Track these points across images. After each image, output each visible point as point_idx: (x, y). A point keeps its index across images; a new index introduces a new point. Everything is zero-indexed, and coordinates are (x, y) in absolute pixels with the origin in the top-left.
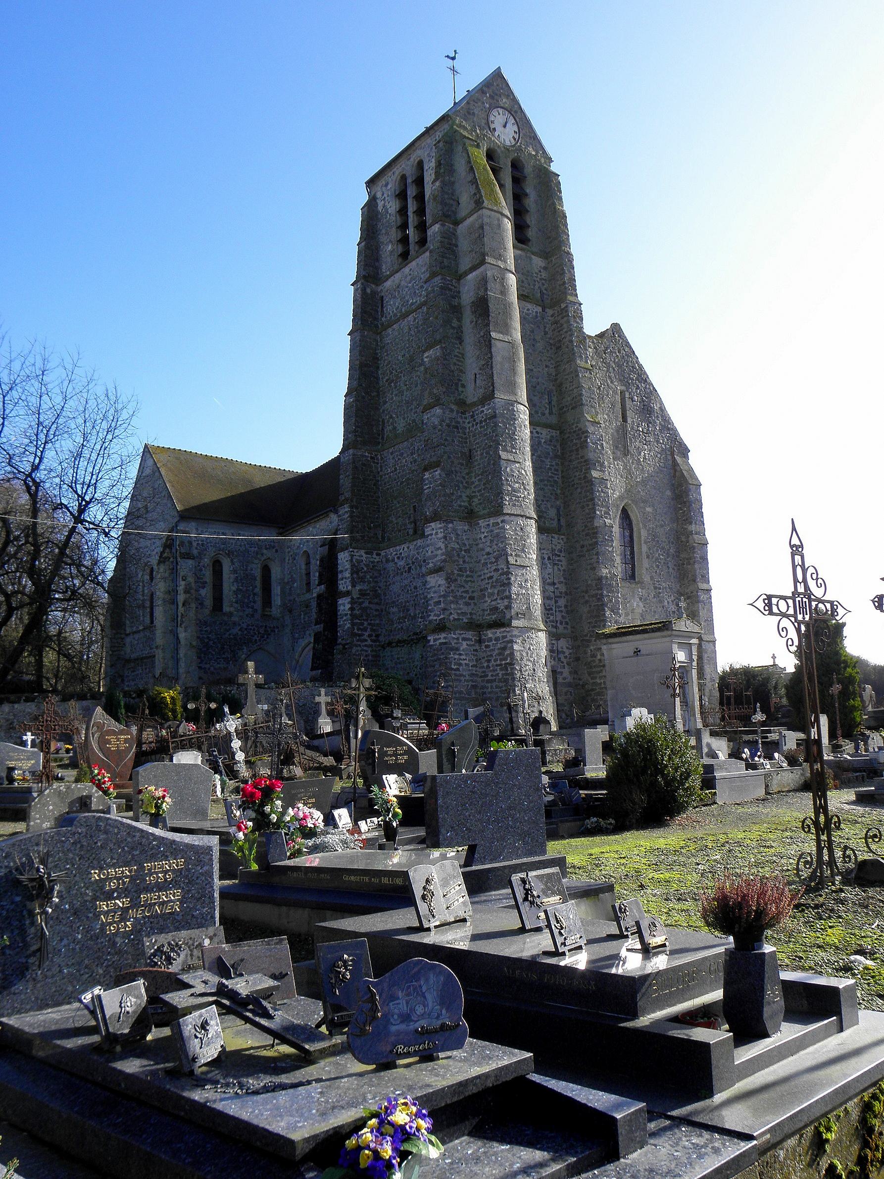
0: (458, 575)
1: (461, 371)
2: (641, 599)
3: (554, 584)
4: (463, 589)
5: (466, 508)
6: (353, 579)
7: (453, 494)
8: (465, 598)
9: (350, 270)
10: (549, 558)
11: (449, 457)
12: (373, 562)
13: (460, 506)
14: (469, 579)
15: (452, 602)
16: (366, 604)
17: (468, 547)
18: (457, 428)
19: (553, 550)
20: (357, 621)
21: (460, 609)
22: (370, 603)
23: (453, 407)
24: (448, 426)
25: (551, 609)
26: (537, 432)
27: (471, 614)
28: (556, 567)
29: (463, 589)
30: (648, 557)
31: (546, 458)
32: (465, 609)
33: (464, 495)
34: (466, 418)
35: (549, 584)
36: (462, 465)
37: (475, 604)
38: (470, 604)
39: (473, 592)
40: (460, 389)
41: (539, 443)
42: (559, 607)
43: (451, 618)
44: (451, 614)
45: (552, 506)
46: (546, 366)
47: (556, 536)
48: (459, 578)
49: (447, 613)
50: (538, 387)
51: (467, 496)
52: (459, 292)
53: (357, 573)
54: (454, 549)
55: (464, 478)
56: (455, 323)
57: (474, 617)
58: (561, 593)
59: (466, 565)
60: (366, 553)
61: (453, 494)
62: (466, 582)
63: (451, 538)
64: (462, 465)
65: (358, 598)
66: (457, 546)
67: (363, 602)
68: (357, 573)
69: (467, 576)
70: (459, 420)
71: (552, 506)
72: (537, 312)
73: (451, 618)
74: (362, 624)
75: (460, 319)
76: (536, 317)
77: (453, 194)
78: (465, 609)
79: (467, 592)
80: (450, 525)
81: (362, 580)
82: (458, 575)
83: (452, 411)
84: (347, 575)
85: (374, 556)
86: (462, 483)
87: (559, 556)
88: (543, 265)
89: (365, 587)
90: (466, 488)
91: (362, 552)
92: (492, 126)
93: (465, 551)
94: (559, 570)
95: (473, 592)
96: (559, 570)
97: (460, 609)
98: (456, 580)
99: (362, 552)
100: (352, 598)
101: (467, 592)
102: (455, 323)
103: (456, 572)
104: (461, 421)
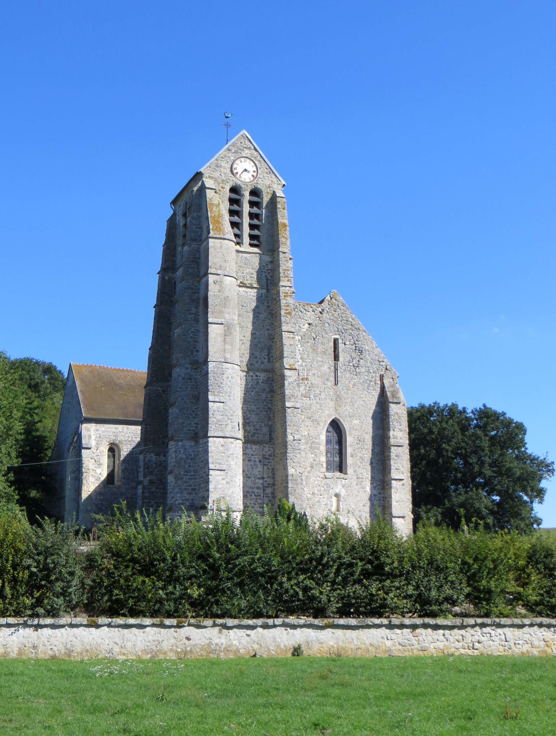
0: (184, 475)
1: (197, 342)
2: (343, 486)
3: (263, 478)
4: (187, 484)
5: (194, 430)
6: (144, 473)
7: (183, 423)
8: (188, 490)
9: (157, 263)
10: (260, 461)
11: (182, 399)
12: (161, 461)
13: (189, 430)
14: (193, 477)
15: (178, 493)
16: (154, 489)
17: (193, 456)
18: (190, 379)
19: (263, 455)
20: (147, 500)
21: (184, 497)
22: (156, 488)
23: (187, 365)
24: (183, 378)
25: (260, 495)
26: (257, 376)
27: (192, 500)
28: (265, 467)
29: (187, 484)
30: (352, 456)
31: (262, 392)
32: (188, 497)
33: (192, 423)
34: (198, 372)
35: (259, 478)
36: (192, 403)
37: (196, 494)
38: (192, 494)
39: (195, 486)
40: (195, 353)
41: (258, 383)
42: (267, 494)
43: (177, 502)
44: (177, 500)
45: (265, 425)
46: (267, 330)
47: (267, 446)
48: (185, 477)
49: (174, 499)
50: (259, 345)
51: (196, 423)
52: (199, 289)
53: (148, 468)
54: (181, 458)
55: (193, 411)
56: (193, 310)
57: (194, 502)
58: (269, 484)
59: (192, 469)
60: (155, 455)
61: (183, 423)
62: (190, 479)
63: (180, 452)
64: (192, 403)
65: (147, 485)
66: (184, 456)
67: (151, 488)
68: (148, 468)
69: (191, 476)
70: (193, 374)
71: (265, 425)
72: (262, 293)
73: (177, 502)
74: (150, 503)
75: (197, 308)
76: (262, 297)
77: (199, 225)
78: (188, 497)
79: (190, 486)
80: (180, 443)
81: (151, 473)
82: (184, 475)
83: (187, 368)
84: (142, 470)
85: (162, 456)
86: (192, 415)
87: (269, 459)
88: (270, 260)
89: (153, 477)
90: (195, 418)
91: (152, 455)
92: (235, 171)
93: (191, 459)
94: (268, 468)
95: (195, 486)
96: (268, 468)
97: (184, 497)
98: (182, 478)
99: (152, 455)
100: (144, 486)
101: (190, 486)
102: (193, 310)
103: (182, 473)
104: (194, 374)
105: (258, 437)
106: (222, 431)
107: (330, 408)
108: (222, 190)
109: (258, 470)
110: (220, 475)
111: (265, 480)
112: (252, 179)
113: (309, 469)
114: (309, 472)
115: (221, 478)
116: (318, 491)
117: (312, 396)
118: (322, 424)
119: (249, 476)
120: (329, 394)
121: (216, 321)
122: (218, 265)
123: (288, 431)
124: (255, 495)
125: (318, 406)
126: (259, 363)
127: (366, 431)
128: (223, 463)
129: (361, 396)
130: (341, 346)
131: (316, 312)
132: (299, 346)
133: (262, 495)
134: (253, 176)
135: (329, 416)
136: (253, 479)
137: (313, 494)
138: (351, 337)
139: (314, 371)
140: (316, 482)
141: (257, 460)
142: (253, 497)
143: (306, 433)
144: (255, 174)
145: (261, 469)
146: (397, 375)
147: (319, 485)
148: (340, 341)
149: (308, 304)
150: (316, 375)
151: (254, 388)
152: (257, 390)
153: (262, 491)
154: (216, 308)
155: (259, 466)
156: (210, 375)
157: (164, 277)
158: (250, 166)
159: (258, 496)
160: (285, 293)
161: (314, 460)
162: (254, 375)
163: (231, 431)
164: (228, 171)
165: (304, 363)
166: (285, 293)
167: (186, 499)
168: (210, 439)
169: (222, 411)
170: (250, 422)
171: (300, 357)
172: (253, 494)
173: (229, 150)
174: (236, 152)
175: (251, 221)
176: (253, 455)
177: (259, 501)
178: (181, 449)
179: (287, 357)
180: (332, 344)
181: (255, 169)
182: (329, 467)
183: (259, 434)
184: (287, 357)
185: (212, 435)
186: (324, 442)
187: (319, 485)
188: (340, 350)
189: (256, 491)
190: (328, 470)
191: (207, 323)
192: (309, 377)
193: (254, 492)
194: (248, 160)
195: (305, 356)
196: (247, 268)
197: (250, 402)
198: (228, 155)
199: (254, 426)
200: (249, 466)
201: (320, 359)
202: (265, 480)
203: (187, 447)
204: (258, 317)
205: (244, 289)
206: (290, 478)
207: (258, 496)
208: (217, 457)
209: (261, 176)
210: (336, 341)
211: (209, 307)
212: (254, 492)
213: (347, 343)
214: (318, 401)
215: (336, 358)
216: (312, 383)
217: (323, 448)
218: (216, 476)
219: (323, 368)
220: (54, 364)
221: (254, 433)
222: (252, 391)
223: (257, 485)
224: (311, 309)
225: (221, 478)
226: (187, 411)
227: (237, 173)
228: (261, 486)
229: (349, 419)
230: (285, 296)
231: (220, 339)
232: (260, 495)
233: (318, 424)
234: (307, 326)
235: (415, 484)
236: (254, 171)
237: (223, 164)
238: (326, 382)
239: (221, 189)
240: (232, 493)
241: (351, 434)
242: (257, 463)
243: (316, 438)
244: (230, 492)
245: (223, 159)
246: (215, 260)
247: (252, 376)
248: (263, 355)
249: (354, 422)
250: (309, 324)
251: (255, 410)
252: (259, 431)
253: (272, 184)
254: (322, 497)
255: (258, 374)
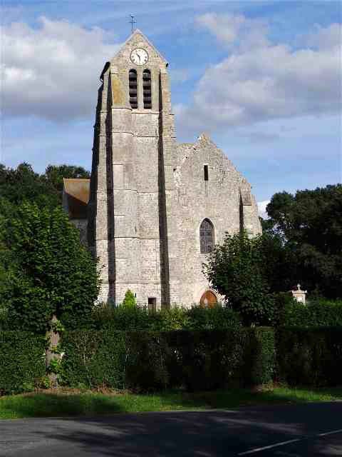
106: (124, 233)
139: (191, 189)
156: (115, 199)
158: (143, 54)
173: (128, 44)
175: (132, 90)
180: (203, 169)
186: (199, 235)
188: (209, 172)
190: (202, 252)
194: (142, 50)
205: (140, 138)
206: (170, 260)
215: (206, 178)
219: (197, 186)
220: (278, 192)
225: (123, 263)
235: (206, 301)
246: (117, 123)
253: (159, 66)
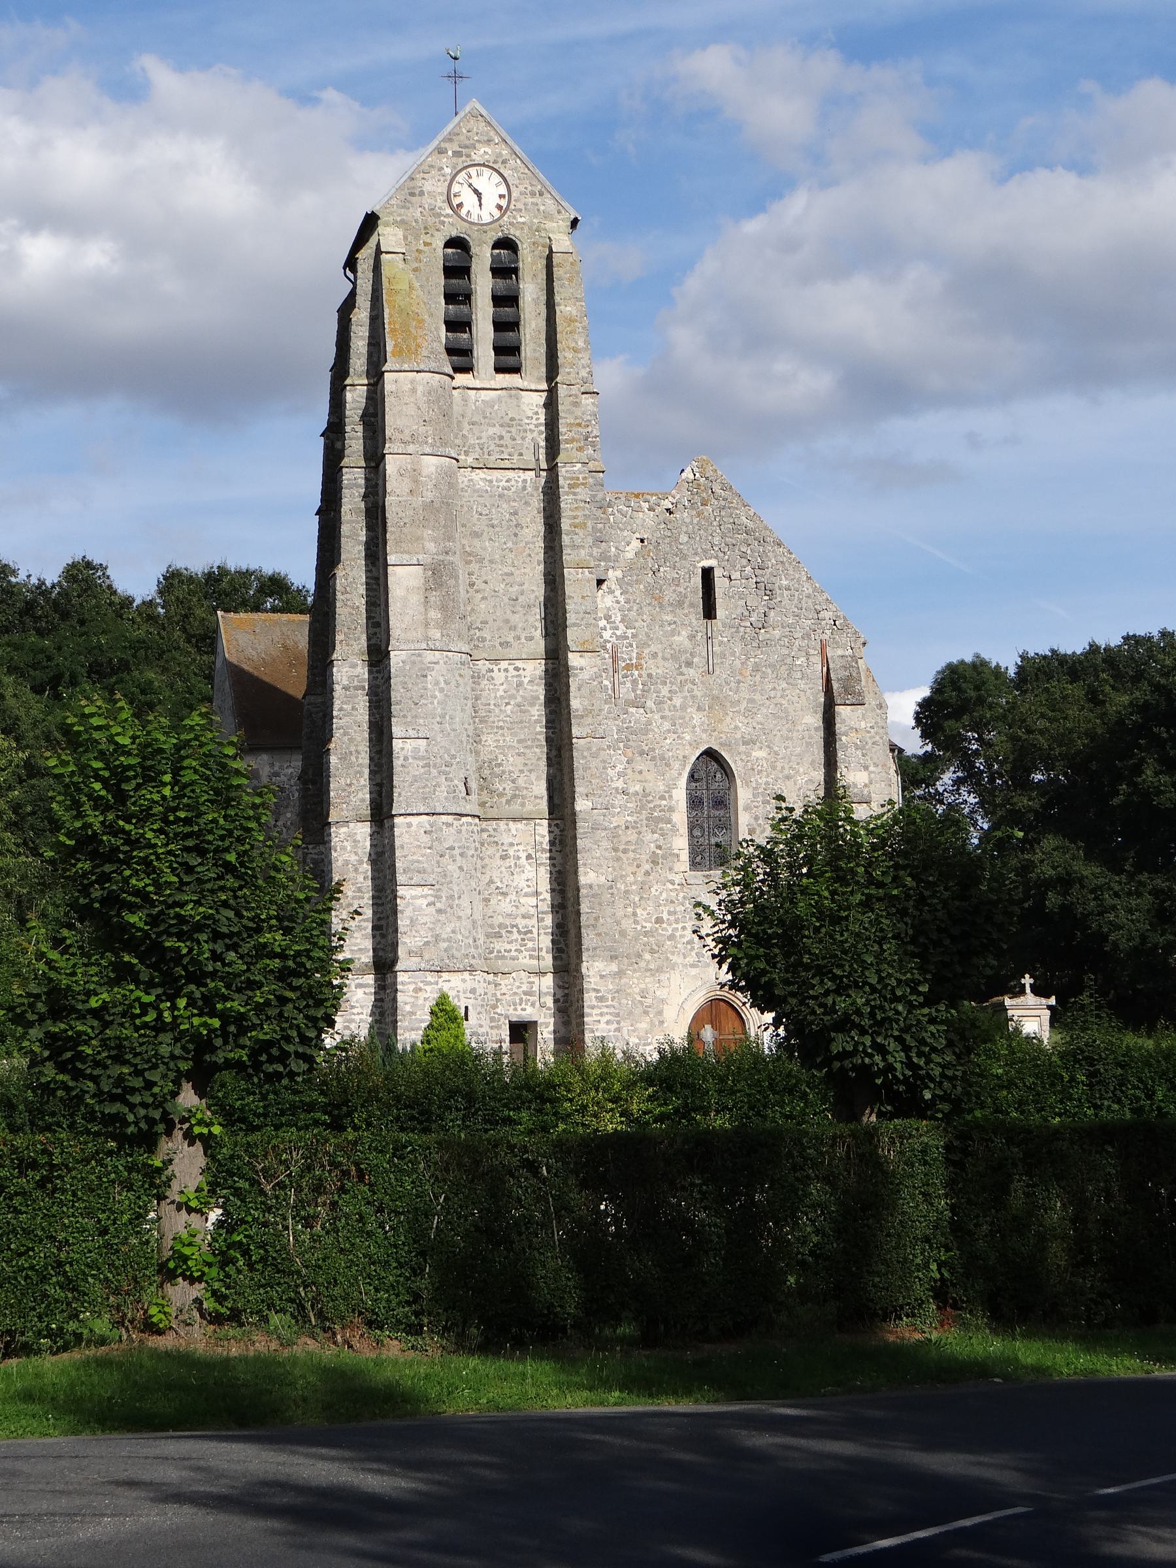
10: (529, 857)
25: (531, 932)
35: (526, 895)
105: (523, 805)
107: (694, 727)
108: (426, 249)
109: (524, 876)
110: (422, 896)
111: (541, 897)
112: (497, 214)
113: (647, 867)
114: (647, 873)
115: (425, 902)
116: (670, 913)
117: (650, 704)
118: (676, 765)
119: (504, 890)
120: (693, 697)
121: (406, 558)
122: (407, 432)
123: (577, 789)
124: (519, 932)
125: (667, 725)
126: (523, 640)
127: (786, 772)
128: (429, 870)
129: (772, 694)
130: (720, 584)
131: (658, 510)
132: (618, 593)
133: (535, 931)
134: (499, 207)
135: (694, 744)
136: (513, 897)
137: (659, 920)
138: (744, 562)
140: (664, 895)
141: (523, 855)
142: (516, 936)
143: (638, 788)
144: (504, 203)
145: (532, 875)
146: (862, 640)
147: (672, 902)
148: (718, 573)
149: (637, 496)
150: (660, 655)
151: (513, 697)
152: (519, 699)
153: (534, 921)
154: (405, 530)
155: (528, 867)
157: (333, 445)
158: (490, 186)
159: (526, 933)
160: (572, 479)
161: (659, 847)
162: (511, 668)
163: (446, 798)
164: (440, 202)
165: (629, 632)
166: (572, 479)
167: (360, 950)
168: (397, 820)
169: (423, 758)
170: (504, 772)
171: (619, 619)
172: (515, 930)
174: (457, 154)
176: (512, 845)
177: (530, 945)
178: (345, 843)
179: (575, 625)
180: (698, 580)
181: (503, 190)
182: (698, 859)
183: (524, 797)
184: (575, 625)
185: (403, 812)
187: (672, 902)
189: (521, 923)
190: (694, 865)
191: (386, 565)
192: (643, 662)
193: (516, 926)
195: (633, 614)
196: (489, 425)
197: (502, 728)
198: (439, 164)
199: (513, 782)
200: (503, 869)
201: (669, 618)
202: (541, 897)
203: (358, 837)
204: (516, 535)
206: (583, 892)
207: (526, 933)
208: (415, 858)
209: (520, 206)
210: (707, 574)
211: (390, 529)
212: (516, 926)
213: (736, 575)
214: (667, 713)
215: (709, 611)
216: (650, 676)
217: (681, 817)
218: (413, 897)
221: (514, 796)
222: (507, 704)
223: (523, 910)
224: (646, 505)
226: (357, 758)
227: (460, 205)
228: (533, 911)
229: (742, 748)
230: (571, 486)
231: (416, 599)
232: (531, 932)
233: (668, 765)
234: (638, 544)
236: (501, 196)
237: (428, 187)
238: (684, 669)
239: (422, 247)
240: (453, 932)
241: (747, 783)
242: (523, 861)
243: (662, 798)
244: (449, 930)
245: (426, 176)
246: (399, 423)
247: (506, 670)
248: (531, 619)
249: (754, 754)
250: (642, 541)
251: (515, 744)
252: (525, 792)
253: (544, 224)
254: (680, 926)
255: (519, 664)
